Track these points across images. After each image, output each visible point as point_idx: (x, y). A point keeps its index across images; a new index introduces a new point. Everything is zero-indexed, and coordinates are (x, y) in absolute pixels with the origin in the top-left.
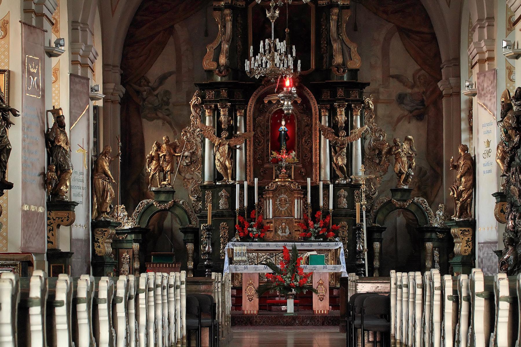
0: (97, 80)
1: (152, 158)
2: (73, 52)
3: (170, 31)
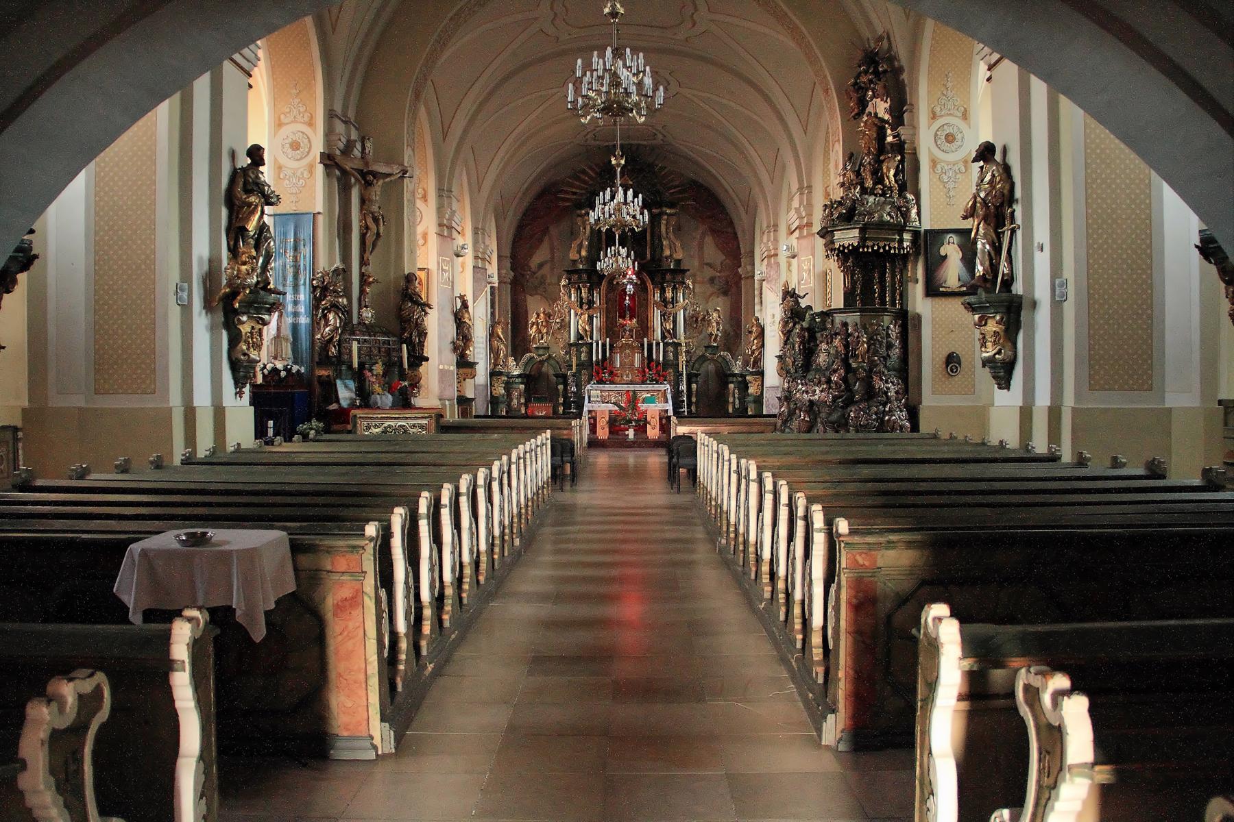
0: (493, 270)
1: (533, 324)
2: (475, 250)
3: (546, 231)
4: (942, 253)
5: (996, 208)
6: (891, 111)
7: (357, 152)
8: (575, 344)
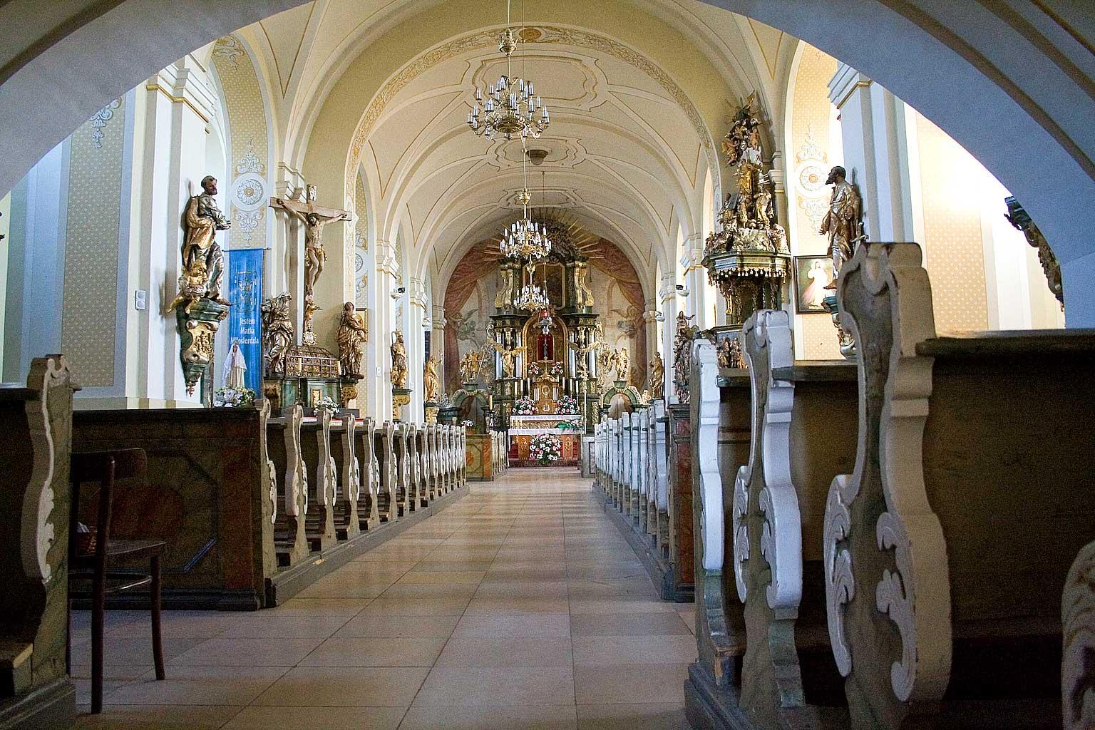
4: (810, 276)
5: (849, 221)
6: (762, 157)
7: (303, 199)
8: (501, 381)
